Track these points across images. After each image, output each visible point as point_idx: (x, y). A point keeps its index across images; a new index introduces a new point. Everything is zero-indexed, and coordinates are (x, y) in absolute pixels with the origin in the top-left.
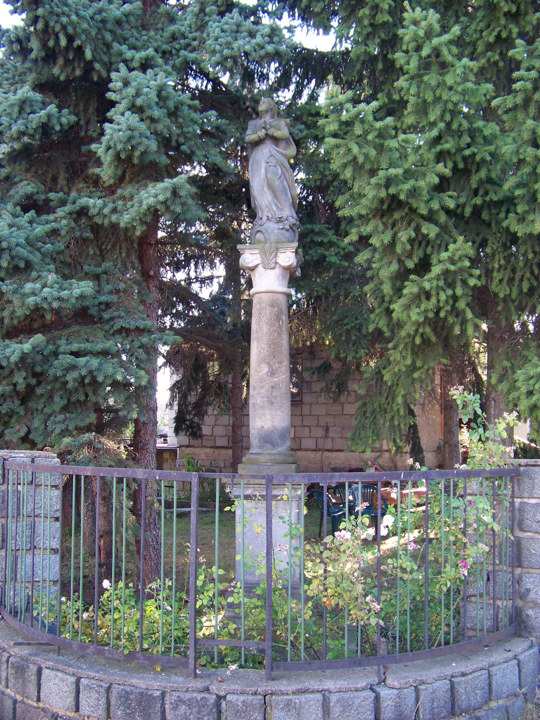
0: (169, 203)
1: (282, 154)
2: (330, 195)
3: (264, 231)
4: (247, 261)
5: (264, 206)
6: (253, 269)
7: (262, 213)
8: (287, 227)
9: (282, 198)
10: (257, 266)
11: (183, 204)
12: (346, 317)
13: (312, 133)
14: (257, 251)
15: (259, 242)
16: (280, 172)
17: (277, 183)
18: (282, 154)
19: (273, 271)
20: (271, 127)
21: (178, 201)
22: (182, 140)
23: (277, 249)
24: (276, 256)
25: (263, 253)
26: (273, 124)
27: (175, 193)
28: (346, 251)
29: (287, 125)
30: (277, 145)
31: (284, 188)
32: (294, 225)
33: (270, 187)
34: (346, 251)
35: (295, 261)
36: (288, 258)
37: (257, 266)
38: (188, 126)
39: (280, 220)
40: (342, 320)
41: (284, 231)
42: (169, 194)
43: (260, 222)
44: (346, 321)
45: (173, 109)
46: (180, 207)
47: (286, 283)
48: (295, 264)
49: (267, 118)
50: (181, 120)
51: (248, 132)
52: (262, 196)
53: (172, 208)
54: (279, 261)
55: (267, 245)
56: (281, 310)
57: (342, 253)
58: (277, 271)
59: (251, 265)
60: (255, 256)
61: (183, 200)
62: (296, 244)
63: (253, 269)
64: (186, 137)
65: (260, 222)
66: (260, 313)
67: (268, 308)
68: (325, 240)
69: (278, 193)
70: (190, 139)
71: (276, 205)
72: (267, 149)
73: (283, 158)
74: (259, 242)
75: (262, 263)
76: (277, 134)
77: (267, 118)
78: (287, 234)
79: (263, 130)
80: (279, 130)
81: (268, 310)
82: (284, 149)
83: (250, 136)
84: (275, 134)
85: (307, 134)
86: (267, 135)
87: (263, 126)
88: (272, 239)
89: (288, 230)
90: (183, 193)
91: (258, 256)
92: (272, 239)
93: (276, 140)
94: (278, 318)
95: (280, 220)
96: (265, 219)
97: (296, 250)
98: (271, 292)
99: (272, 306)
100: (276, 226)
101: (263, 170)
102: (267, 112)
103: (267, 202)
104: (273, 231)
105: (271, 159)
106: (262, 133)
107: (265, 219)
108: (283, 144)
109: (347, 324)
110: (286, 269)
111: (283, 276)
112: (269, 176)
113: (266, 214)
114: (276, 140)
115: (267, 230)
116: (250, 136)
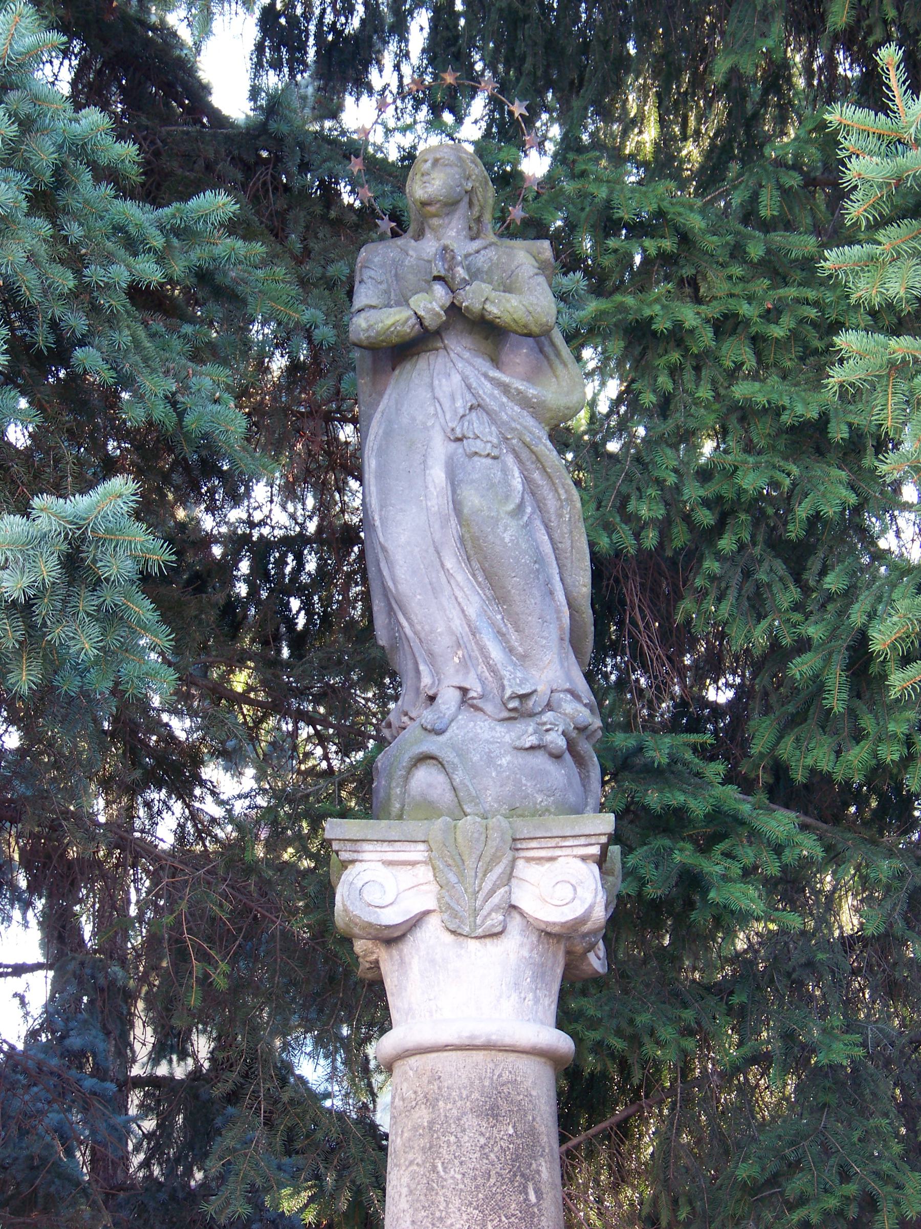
0: (42, 609)
1: (525, 402)
2: (702, 594)
3: (449, 756)
4: (373, 896)
5: (442, 643)
6: (393, 937)
7: (437, 674)
8: (557, 740)
9: (530, 604)
10: (416, 922)
11: (110, 618)
12: (794, 1166)
13: (622, 308)
14: (417, 852)
15: (427, 809)
16: (517, 482)
17: (508, 533)
18: (525, 402)
19: (493, 948)
20: (475, 274)
21: (86, 603)
22: (78, 322)
23: (516, 843)
24: (509, 877)
25: (448, 862)
26: (481, 261)
27: (76, 563)
28: (789, 856)
29: (543, 267)
30: (496, 361)
31: (539, 559)
32: (582, 730)
33: (476, 551)
34: (789, 856)
35: (601, 898)
36: (567, 885)
37: (416, 922)
38: (109, 259)
39: (520, 708)
40: (774, 1180)
41: (540, 760)
42: (48, 569)
43: (427, 716)
44: (796, 1185)
45: (47, 177)
46: (95, 630)
47: (549, 1005)
48: (600, 915)
49: (453, 233)
50: (75, 231)
51: (364, 296)
52: (435, 591)
53: (57, 634)
54: (525, 899)
55: (469, 824)
56: (532, 1133)
57: (773, 869)
58: (514, 947)
59: (391, 917)
60: (406, 876)
61: (110, 597)
62: (606, 823)
63: (393, 937)
64: (94, 309)
65: (427, 716)
66: (431, 1149)
67: (470, 1121)
68: (698, 807)
69: (514, 583)
70: (112, 320)
71: (501, 635)
72: (450, 380)
73: (530, 422)
74: (427, 809)
75: (446, 907)
76: (504, 307)
77: (453, 233)
78: (559, 775)
79: (439, 290)
80: (508, 289)
81: (474, 1131)
82: (532, 377)
83: (377, 315)
84: (493, 310)
85: (601, 315)
86: (454, 310)
87: (439, 268)
88: (490, 797)
89: (556, 757)
90: (118, 566)
91: (424, 873)
92: (490, 797)
93: (490, 333)
94: (519, 1171)
95: (520, 708)
96: (449, 699)
97: (604, 848)
98: (488, 1047)
99: (491, 1112)
100: (506, 735)
101: (438, 475)
102: (450, 205)
103: (458, 624)
104: (490, 760)
105: (478, 424)
106: (431, 303)
107: (449, 699)
108: (520, 356)
109: (802, 1200)
110: (549, 935)
111: (540, 974)
112: (473, 499)
113: (452, 678)
114: (490, 333)
115: (462, 754)
116: (377, 315)
